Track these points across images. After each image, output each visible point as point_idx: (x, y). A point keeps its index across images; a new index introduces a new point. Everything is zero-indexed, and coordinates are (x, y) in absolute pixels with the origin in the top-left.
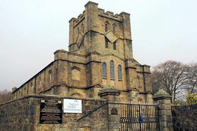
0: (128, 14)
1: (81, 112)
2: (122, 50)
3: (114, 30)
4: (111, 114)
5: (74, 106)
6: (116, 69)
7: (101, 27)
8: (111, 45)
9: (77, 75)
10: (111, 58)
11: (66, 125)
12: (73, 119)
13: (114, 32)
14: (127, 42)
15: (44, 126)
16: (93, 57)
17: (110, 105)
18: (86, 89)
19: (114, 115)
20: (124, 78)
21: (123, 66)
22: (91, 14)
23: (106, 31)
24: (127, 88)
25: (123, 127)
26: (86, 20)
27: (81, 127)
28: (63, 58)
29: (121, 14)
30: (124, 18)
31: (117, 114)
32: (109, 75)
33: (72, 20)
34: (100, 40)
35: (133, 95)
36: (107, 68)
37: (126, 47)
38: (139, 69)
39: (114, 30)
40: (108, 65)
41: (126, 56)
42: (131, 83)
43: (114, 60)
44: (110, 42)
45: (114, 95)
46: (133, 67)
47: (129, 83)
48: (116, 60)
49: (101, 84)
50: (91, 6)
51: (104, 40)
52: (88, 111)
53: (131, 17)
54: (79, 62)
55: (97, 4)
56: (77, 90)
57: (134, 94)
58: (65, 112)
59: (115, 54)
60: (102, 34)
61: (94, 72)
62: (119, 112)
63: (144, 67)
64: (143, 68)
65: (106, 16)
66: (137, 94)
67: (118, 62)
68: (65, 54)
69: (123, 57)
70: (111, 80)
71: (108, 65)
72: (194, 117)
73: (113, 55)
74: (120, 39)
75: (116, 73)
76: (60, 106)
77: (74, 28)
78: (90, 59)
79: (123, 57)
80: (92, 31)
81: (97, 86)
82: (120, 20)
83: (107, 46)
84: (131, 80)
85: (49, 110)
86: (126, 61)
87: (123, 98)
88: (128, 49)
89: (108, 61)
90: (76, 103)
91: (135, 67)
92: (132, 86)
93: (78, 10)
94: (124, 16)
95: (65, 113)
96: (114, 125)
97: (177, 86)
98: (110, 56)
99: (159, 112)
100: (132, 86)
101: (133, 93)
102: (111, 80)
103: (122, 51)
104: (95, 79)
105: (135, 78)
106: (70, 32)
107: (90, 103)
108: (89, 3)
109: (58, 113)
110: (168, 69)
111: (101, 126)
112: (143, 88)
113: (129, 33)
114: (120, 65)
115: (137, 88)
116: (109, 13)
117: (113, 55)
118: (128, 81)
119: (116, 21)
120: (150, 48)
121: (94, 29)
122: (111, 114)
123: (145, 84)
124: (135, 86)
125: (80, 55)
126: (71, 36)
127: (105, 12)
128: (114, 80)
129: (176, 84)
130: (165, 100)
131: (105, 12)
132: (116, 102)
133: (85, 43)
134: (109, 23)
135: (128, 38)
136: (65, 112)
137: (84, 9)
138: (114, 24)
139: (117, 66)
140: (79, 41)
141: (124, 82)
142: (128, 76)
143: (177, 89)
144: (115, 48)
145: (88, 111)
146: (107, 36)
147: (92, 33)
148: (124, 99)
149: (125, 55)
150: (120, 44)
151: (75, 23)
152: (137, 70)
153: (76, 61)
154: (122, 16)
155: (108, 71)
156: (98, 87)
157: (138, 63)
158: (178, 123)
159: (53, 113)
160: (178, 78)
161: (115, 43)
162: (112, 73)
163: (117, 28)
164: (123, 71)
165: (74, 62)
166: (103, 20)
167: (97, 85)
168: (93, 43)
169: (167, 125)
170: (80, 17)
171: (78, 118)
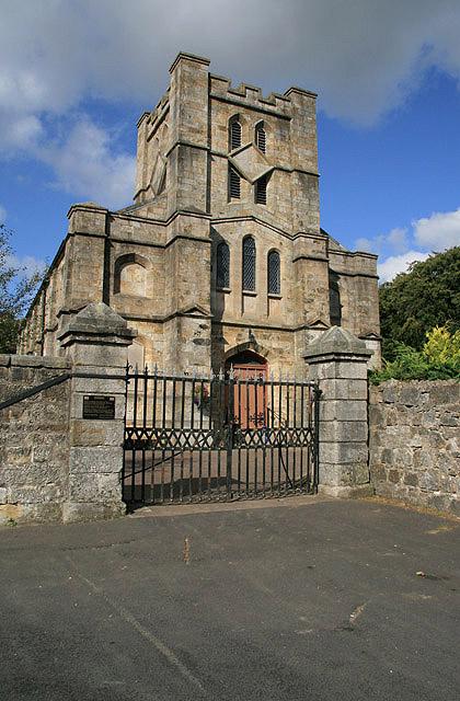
0: (309, 94)
4: (85, 417)
8: (246, 188)
10: (247, 227)
14: (301, 179)
19: (97, 424)
25: (134, 473)
26: (171, 113)
28: (91, 230)
31: (111, 417)
45: (102, 343)
50: (186, 68)
54: (143, 241)
59: (261, 217)
65: (238, 98)
68: (98, 216)
70: (244, 294)
72: (438, 435)
73: (254, 219)
74: (281, 169)
77: (148, 141)
80: (183, 144)
83: (234, 191)
89: (233, 237)
99: (321, 407)
104: (188, 293)
111: (36, 461)
117: (254, 219)
122: (85, 417)
124: (322, 314)
144: (260, 197)
146: (235, 160)
148: (285, 354)
153: (135, 238)
158: (386, 450)
163: (272, 136)
165: (125, 242)
167: (192, 310)
169: (343, 455)
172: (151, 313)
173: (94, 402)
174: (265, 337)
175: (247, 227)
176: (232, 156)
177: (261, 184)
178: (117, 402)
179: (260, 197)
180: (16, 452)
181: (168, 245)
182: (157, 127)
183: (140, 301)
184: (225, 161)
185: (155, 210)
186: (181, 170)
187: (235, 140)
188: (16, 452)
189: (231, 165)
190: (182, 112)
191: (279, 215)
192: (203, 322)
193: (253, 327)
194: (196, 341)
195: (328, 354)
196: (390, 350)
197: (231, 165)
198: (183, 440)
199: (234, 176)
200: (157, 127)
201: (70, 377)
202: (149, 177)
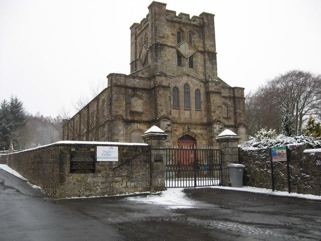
1: (117, 160)
2: (201, 68)
3: (190, 39)
5: (110, 153)
6: (193, 95)
7: (171, 36)
8: (187, 62)
9: (138, 105)
10: (185, 79)
11: (100, 175)
12: (107, 168)
13: (190, 43)
14: (208, 55)
15: (76, 176)
16: (158, 81)
17: (153, 152)
20: (203, 106)
21: (202, 90)
22: (155, 19)
23: (179, 41)
24: (208, 120)
26: (150, 28)
27: (117, 177)
29: (201, 15)
30: (206, 21)
32: (182, 104)
33: (134, 27)
34: (169, 55)
35: (215, 130)
37: (208, 64)
38: (225, 93)
39: (190, 39)
40: (181, 90)
41: (207, 75)
42: (213, 114)
43: (189, 82)
48: (191, 81)
49: (170, 117)
51: (175, 56)
52: (126, 158)
53: (215, 18)
55: (165, 5)
56: (138, 125)
57: (218, 129)
58: (98, 160)
61: (161, 101)
62: (164, 159)
63: (236, 90)
64: (234, 92)
65: (179, 20)
66: (221, 128)
67: (195, 85)
71: (181, 90)
73: (188, 75)
75: (193, 101)
76: (94, 155)
78: (155, 84)
79: (202, 77)
80: (157, 45)
82: (200, 24)
83: (180, 63)
84: (213, 110)
85: (81, 159)
86: (206, 82)
87: (202, 134)
88: (211, 66)
89: (180, 86)
90: (111, 150)
92: (214, 118)
93: (141, 14)
94: (205, 18)
95: (98, 162)
96: (158, 174)
97: (305, 109)
101: (216, 128)
102: (185, 110)
103: (201, 69)
104: (162, 111)
105: (219, 107)
106: (132, 43)
107: (129, 150)
108: (154, 3)
109: (91, 162)
110: (290, 84)
112: (233, 119)
113: (212, 43)
115: (221, 120)
116: (183, 16)
117: (188, 75)
118: (208, 110)
119: (194, 25)
120: (246, 64)
121: (160, 41)
123: (235, 113)
125: (141, 78)
127: (177, 15)
129: (303, 107)
131: (177, 15)
132: (161, 148)
133: (150, 61)
134: (182, 31)
135: (211, 49)
136: (98, 160)
137: (147, 11)
138: (190, 31)
139: (194, 91)
140: (143, 57)
141: (204, 113)
142: (209, 104)
143: (304, 114)
145: (126, 158)
147: (157, 48)
148: (204, 136)
150: (199, 60)
151: (137, 30)
152: (222, 95)
154: (202, 18)
155: (182, 99)
159: (84, 162)
160: (306, 98)
161: (191, 59)
163: (195, 36)
164: (203, 98)
166: (174, 27)
168: (159, 61)
170: (143, 23)
171: (114, 167)
172: (144, 118)
174: (195, 129)
175: (185, 79)
177: (191, 59)
180: (137, 172)
182: (142, 32)
183: (140, 114)
184: (175, 50)
185: (145, 73)
186: (156, 56)
188: (137, 172)
190: (155, 30)
192: (168, 123)
197: (178, 53)
198: (175, 168)
199: (180, 56)
200: (142, 32)
202: (138, 55)
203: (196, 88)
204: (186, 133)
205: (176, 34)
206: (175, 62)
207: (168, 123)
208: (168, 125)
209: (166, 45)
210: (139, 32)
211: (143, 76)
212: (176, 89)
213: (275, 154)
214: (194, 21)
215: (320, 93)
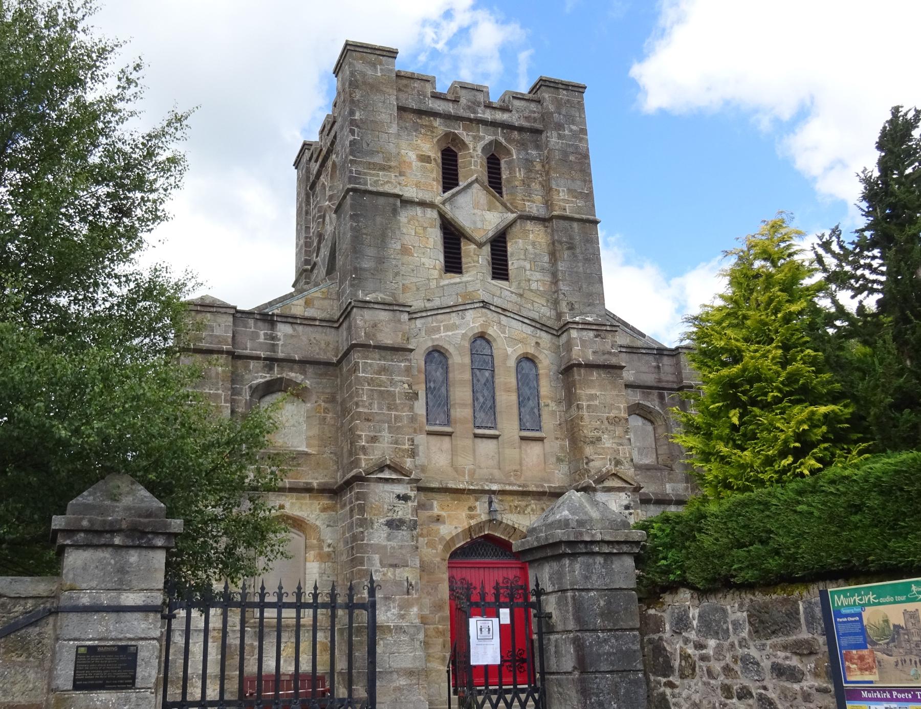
0: (567, 86)
2: (538, 276)
4: (76, 687)
8: (477, 260)
10: (473, 321)
16: (359, 323)
18: (334, 492)
20: (550, 421)
21: (547, 362)
32: (462, 412)
36: (451, 375)
40: (460, 360)
42: (588, 450)
44: (470, 239)
46: (600, 360)
47: (581, 450)
49: (408, 463)
51: (435, 236)
55: (392, 54)
59: (497, 301)
60: (423, 204)
65: (450, 108)
66: (627, 507)
69: (543, 311)
70: (476, 436)
71: (460, 360)
73: (485, 305)
75: (507, 399)
81: (386, 475)
91: (614, 361)
98: (469, 315)
100: (596, 465)
102: (476, 436)
103: (538, 281)
113: (578, 185)
114: (528, 359)
116: (463, 93)
117: (485, 305)
119: (508, 127)
122: (76, 687)
125: (308, 321)
126: (414, 247)
128: (496, 437)
130: (373, 486)
135: (565, 202)
139: (512, 363)
141: (555, 445)
142: (574, 411)
144: (500, 270)
146: (447, 208)
149: (556, 303)
150: (527, 247)
152: (629, 375)
156: (387, 480)
157: (644, 336)
161: (498, 245)
162: (485, 404)
164: (547, 388)
166: (431, 128)
167: (381, 469)
173: (96, 659)
175: (473, 321)
176: (444, 203)
177: (498, 245)
178: (141, 655)
179: (500, 270)
181: (340, 362)
182: (323, 165)
183: (298, 457)
184: (433, 214)
187: (450, 179)
189: (442, 216)
191: (528, 294)
192: (401, 489)
193: (494, 492)
194: (390, 524)
195: (618, 543)
196: (649, 558)
197: (442, 216)
199: (453, 238)
200: (323, 165)
201: (55, 612)
203: (520, 350)
204: (480, 526)
205: (436, 155)
206: (435, 257)
207: (401, 489)
208: (398, 497)
209: (407, 203)
210: (315, 167)
211: (310, 313)
212: (437, 355)
213: (862, 637)
214: (505, 109)
215: (919, 512)
